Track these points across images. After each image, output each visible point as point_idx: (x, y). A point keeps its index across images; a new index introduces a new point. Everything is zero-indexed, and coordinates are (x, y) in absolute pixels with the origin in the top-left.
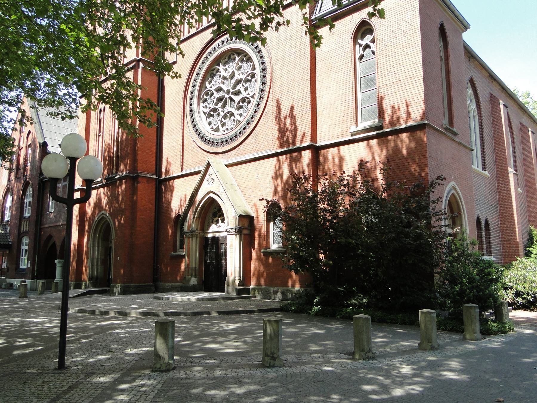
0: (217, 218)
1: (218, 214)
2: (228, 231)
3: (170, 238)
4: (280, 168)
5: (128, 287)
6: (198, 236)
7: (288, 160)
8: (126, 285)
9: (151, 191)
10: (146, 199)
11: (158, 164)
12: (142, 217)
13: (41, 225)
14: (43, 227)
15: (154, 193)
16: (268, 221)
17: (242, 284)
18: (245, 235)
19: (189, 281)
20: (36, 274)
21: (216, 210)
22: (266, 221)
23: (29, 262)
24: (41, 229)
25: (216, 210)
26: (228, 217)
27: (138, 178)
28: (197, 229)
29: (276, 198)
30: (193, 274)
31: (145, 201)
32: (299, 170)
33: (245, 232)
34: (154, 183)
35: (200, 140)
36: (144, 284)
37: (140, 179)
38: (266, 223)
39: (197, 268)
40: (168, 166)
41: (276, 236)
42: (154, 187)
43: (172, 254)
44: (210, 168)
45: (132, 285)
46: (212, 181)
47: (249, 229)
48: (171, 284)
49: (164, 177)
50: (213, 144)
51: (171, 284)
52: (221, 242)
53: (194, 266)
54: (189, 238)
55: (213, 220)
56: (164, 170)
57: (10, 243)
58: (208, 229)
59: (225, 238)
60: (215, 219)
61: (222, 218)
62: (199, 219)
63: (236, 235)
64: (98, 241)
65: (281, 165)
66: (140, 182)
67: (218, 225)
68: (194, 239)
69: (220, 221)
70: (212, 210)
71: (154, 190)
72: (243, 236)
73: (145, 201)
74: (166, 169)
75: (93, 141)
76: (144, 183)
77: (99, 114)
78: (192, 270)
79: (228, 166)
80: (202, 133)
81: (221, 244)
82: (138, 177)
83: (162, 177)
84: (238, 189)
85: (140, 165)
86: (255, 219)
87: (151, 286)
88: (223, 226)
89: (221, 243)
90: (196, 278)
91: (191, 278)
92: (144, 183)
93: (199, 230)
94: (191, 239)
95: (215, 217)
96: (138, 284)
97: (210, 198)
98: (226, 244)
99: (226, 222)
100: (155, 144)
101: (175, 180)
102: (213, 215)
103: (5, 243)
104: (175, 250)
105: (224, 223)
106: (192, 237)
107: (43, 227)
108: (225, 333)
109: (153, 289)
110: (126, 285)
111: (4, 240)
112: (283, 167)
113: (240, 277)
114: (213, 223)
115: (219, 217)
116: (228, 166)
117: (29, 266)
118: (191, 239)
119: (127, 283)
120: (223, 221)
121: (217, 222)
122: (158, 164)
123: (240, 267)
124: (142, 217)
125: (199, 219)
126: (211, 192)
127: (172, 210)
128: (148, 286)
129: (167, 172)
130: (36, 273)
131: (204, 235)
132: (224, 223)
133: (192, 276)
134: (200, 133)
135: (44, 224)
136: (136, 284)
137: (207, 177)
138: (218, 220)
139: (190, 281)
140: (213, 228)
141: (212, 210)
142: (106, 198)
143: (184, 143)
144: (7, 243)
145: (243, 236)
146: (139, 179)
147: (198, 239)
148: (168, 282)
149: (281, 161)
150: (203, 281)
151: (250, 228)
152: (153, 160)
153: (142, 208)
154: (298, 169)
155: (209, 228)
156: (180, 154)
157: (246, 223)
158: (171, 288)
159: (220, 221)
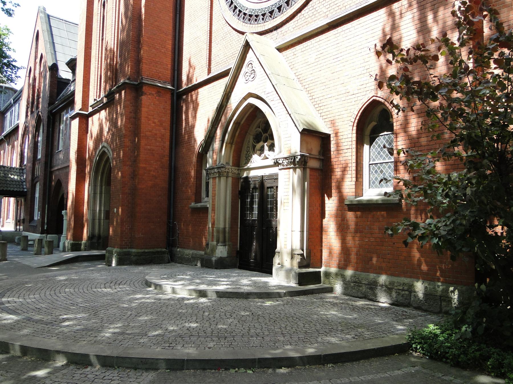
0: (261, 144)
1: (264, 135)
2: (280, 162)
3: (192, 180)
4: (394, 27)
5: (129, 254)
6: (230, 174)
7: (415, 6)
8: (125, 250)
9: (164, 108)
10: (156, 121)
11: (176, 69)
12: (149, 147)
13: (51, 167)
14: (53, 170)
15: (169, 112)
16: (360, 142)
17: (305, 263)
18: (312, 169)
19: (213, 250)
20: (47, 227)
21: (260, 130)
22: (354, 143)
23: (39, 212)
24: (51, 173)
25: (260, 130)
26: (279, 137)
27: (142, 87)
28: (228, 163)
29: (382, 94)
30: (221, 239)
31: (154, 123)
32: (445, 23)
33: (314, 164)
34: (169, 96)
35: (236, 18)
36: (151, 250)
37: (145, 88)
38: (354, 146)
39: (227, 229)
40: (191, 71)
41: (376, 172)
42: (169, 102)
43: (193, 204)
44: (250, 53)
45: (134, 250)
46: (252, 76)
47: (319, 159)
48: (191, 252)
49: (184, 87)
50: (256, 20)
51: (191, 252)
52: (267, 184)
53: (221, 226)
54: (214, 178)
55: (254, 147)
56: (184, 78)
57: (25, 190)
58: (247, 163)
59: (275, 178)
60: (259, 146)
61: (270, 142)
62: (231, 147)
63: (295, 169)
64: (101, 186)
65: (397, 22)
66: (146, 94)
67: (263, 155)
68: (223, 179)
69: (266, 148)
70: (254, 130)
71: (169, 107)
72: (308, 171)
73: (154, 123)
74: (188, 76)
75: (95, 47)
76: (153, 95)
77: (102, 8)
78: (218, 231)
79: (281, 49)
80: (240, 6)
81: (268, 188)
82: (142, 84)
83: (181, 87)
84: (299, 86)
85: (145, 67)
86: (332, 139)
87: (164, 253)
88: (271, 156)
89: (269, 185)
90: (225, 245)
91: (217, 244)
92: (153, 95)
93: (231, 164)
94: (217, 179)
95: (258, 142)
96: (143, 250)
97: (250, 105)
98: (277, 187)
99: (276, 148)
100: (170, 37)
101: (200, 90)
102: (254, 139)
103: (18, 190)
104: (198, 199)
105: (274, 151)
106: (219, 177)
107: (53, 170)
108: (226, 92)
109: (167, 256)
110: (125, 250)
111: (18, 186)
112: (401, 24)
113: (303, 250)
114: (254, 152)
115: (265, 141)
116: (281, 49)
117: (39, 218)
118: (217, 179)
119: (126, 248)
120: (272, 147)
121: (262, 150)
122: (176, 69)
123: (302, 231)
124: (149, 147)
125: (231, 147)
126: (250, 95)
127: (195, 140)
128: (158, 252)
129: (189, 79)
130: (46, 226)
131: (239, 174)
132: (274, 151)
133: (218, 242)
134: (236, 7)
135: (54, 167)
136: (140, 251)
137: (244, 69)
138: (263, 147)
139: (215, 251)
140: (256, 160)
141: (254, 130)
142: (108, 123)
143: (213, 30)
144: (22, 190)
145: (308, 171)
146: (144, 88)
147: (230, 180)
148: (188, 248)
149: (397, 14)
150: (238, 252)
151: (322, 158)
152: (168, 61)
153: (147, 133)
154: (441, 22)
155: (248, 160)
156: (206, 47)
157: (315, 146)
158: (192, 257)
159: (266, 148)
